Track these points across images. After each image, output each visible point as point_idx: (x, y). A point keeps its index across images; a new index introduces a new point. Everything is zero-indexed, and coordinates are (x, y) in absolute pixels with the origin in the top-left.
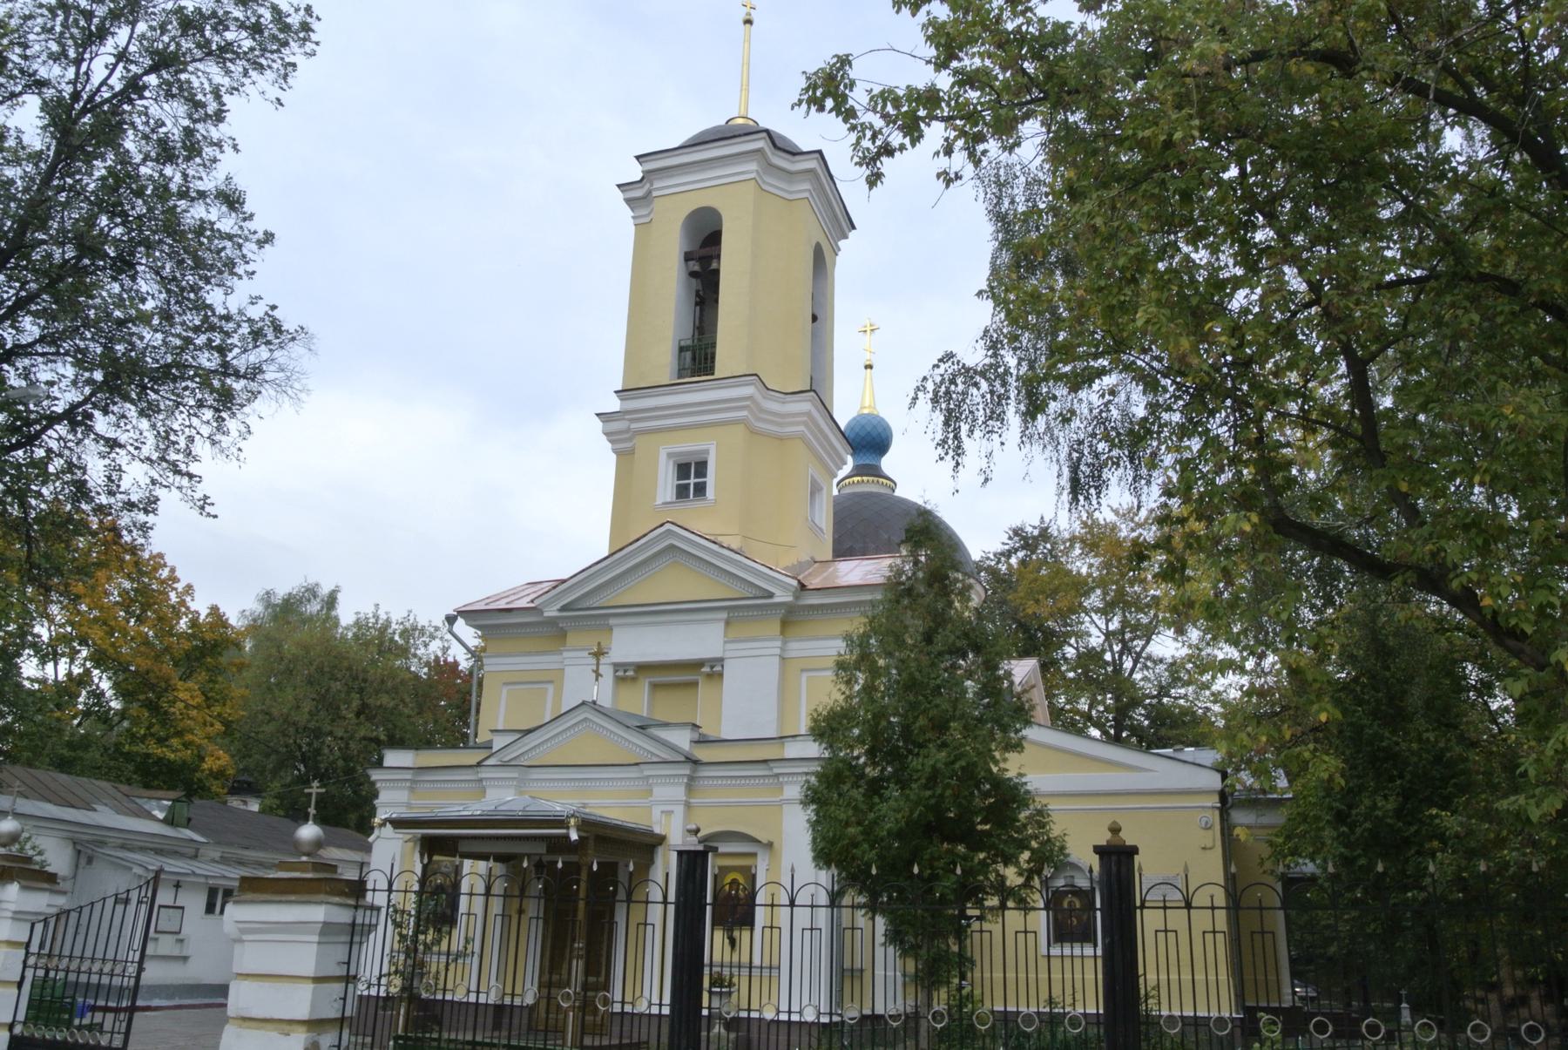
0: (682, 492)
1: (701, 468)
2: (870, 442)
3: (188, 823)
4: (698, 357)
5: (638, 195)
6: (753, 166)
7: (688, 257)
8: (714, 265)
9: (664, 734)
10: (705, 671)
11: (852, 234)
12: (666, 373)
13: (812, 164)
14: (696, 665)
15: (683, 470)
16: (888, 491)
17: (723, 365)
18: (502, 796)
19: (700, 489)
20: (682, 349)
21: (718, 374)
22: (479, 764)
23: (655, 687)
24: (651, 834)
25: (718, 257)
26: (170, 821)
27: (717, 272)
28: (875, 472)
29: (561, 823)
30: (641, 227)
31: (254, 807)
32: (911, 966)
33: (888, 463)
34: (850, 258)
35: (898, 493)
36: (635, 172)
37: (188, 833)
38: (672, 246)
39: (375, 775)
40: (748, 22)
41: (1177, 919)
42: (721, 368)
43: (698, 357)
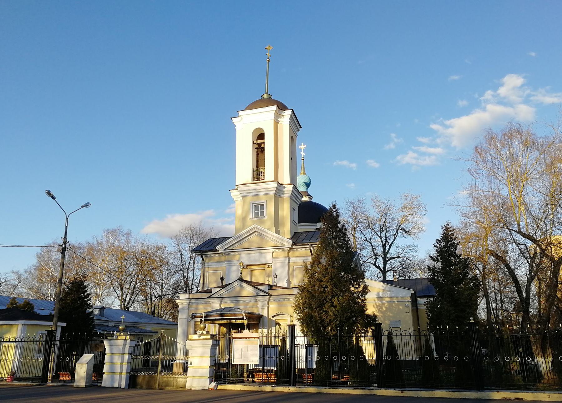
1: (262, 206)
8: (262, 146)
9: (260, 287)
21: (265, 180)
25: (264, 143)
27: (264, 148)
41: (408, 337)
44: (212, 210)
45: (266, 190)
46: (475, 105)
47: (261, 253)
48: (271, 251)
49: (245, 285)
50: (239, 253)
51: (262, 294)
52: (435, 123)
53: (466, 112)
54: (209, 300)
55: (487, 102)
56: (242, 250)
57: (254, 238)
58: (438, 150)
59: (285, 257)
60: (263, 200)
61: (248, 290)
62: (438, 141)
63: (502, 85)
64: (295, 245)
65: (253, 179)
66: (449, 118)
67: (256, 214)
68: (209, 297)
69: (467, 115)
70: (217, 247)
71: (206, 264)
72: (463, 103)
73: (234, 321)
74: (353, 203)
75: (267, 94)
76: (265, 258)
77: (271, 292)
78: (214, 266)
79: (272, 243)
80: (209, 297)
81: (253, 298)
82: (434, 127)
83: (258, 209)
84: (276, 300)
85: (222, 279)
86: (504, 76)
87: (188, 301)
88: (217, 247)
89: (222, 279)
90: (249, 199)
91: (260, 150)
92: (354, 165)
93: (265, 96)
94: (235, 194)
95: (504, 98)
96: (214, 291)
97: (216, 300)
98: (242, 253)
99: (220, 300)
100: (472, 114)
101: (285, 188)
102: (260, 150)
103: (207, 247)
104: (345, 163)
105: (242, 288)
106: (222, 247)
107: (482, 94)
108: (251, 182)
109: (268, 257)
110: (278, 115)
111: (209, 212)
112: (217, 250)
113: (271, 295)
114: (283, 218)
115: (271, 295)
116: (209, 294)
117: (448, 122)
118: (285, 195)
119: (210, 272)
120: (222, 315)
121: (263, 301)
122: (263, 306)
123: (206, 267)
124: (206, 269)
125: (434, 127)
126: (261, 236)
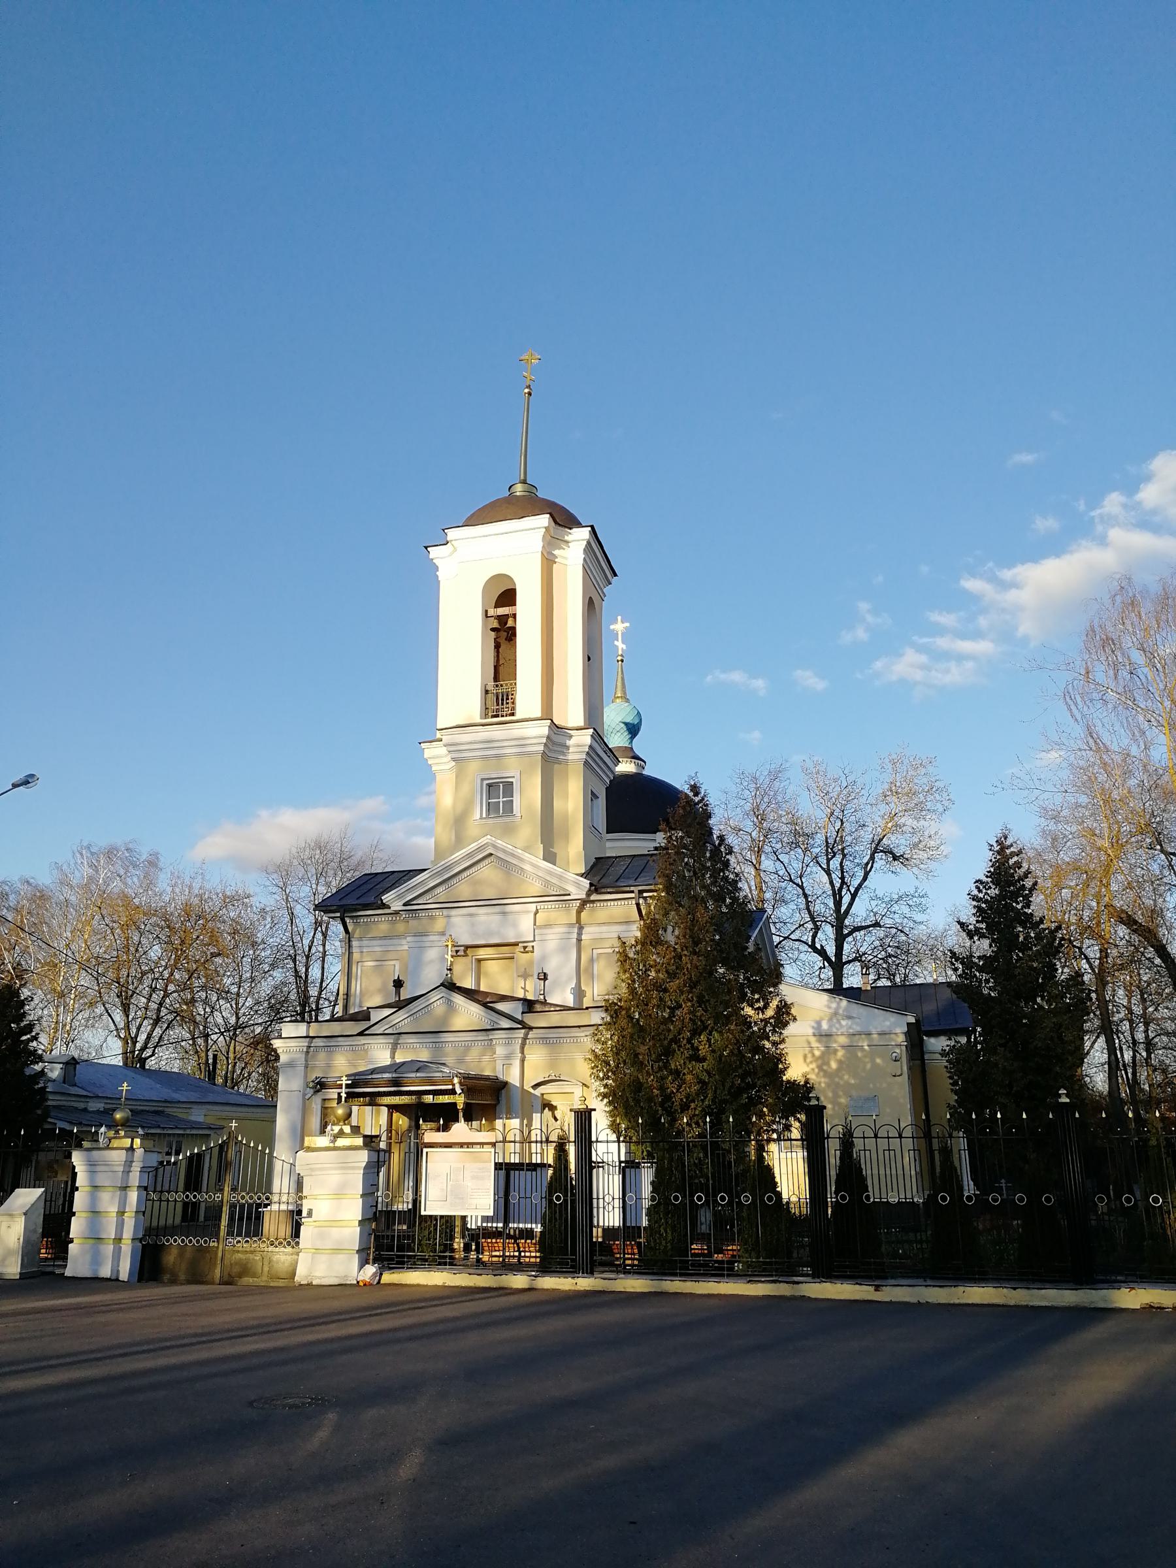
1: (509, 787)
8: (510, 623)
9: (500, 1006)
24: (496, 1080)
27: (514, 629)
44: (382, 798)
45: (521, 742)
46: (1078, 530)
47: (504, 913)
48: (533, 907)
49: (459, 999)
50: (445, 912)
51: (505, 1023)
52: (973, 575)
53: (1054, 546)
54: (363, 1040)
55: (1110, 521)
56: (452, 904)
57: (486, 872)
58: (983, 647)
59: (571, 925)
60: (511, 771)
61: (468, 1014)
62: (983, 622)
63: (1148, 478)
64: (597, 891)
65: (486, 711)
66: (1011, 565)
67: (492, 809)
68: (361, 1034)
69: (1058, 556)
70: (386, 898)
71: (355, 943)
72: (1046, 524)
73: (429, 1099)
74: (755, 779)
75: (524, 482)
76: (515, 925)
77: (530, 1019)
78: (377, 947)
79: (536, 888)
80: (361, 1034)
81: (481, 1036)
82: (973, 585)
83: (498, 792)
84: (545, 1040)
85: (398, 984)
86: (1152, 455)
87: (305, 1043)
88: (386, 898)
89: (398, 984)
90: (474, 767)
91: (503, 634)
92: (759, 683)
93: (519, 489)
94: (437, 755)
95: (1154, 512)
96: (376, 1016)
97: (381, 1040)
98: (454, 912)
99: (391, 1040)
100: (1071, 552)
101: (571, 736)
102: (503, 634)
103: (359, 897)
104: (737, 677)
105: (451, 1007)
106: (400, 897)
107: (1095, 500)
108: (478, 720)
109: (523, 925)
110: (552, 542)
111: (372, 804)
112: (384, 906)
113: (531, 1028)
114: (566, 817)
115: (531, 1028)
116: (363, 1025)
117: (1007, 574)
118: (570, 757)
119: (365, 965)
120: (396, 1082)
121: (509, 1042)
122: (508, 1057)
123: (355, 950)
124: (356, 956)
125: (973, 585)
126: (507, 866)
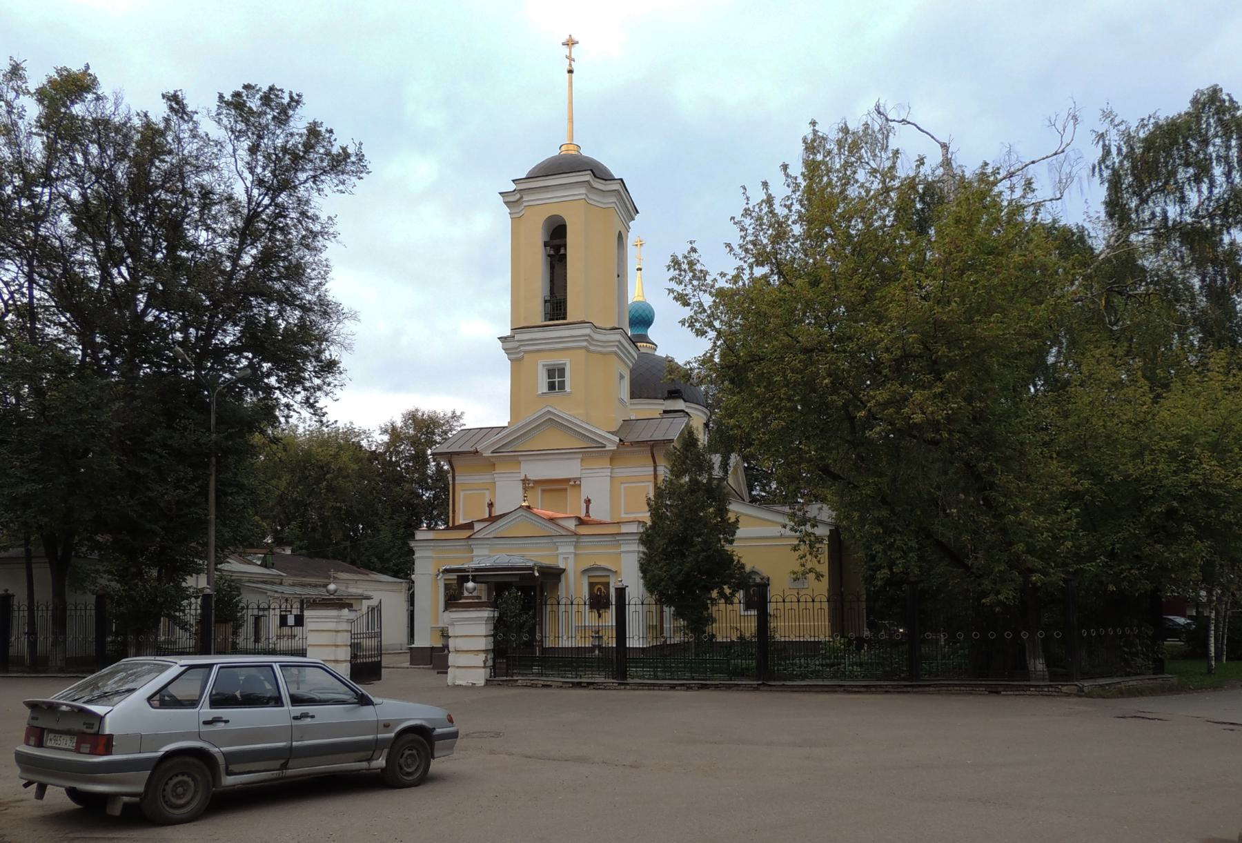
0: (552, 386)
1: (562, 372)
2: (642, 320)
3: (272, 566)
4: (556, 308)
5: (514, 200)
6: (583, 191)
7: (546, 244)
8: (562, 251)
10: (575, 483)
11: (637, 217)
12: (539, 319)
13: (617, 187)
14: (567, 480)
15: (551, 373)
16: (650, 352)
17: (573, 313)
18: (484, 557)
19: (562, 385)
20: (546, 301)
21: (569, 319)
22: (469, 538)
23: (543, 491)
25: (565, 246)
26: (264, 565)
27: (565, 256)
28: (645, 339)
29: (531, 569)
30: (516, 220)
31: (288, 552)
32: (834, 514)
33: (652, 333)
34: (636, 230)
35: (657, 353)
36: (512, 187)
37: (275, 572)
38: (538, 237)
39: (412, 544)
40: (571, 72)
41: (810, 605)
42: (571, 317)
43: (556, 308)
89: (491, 505)
96: (477, 527)
